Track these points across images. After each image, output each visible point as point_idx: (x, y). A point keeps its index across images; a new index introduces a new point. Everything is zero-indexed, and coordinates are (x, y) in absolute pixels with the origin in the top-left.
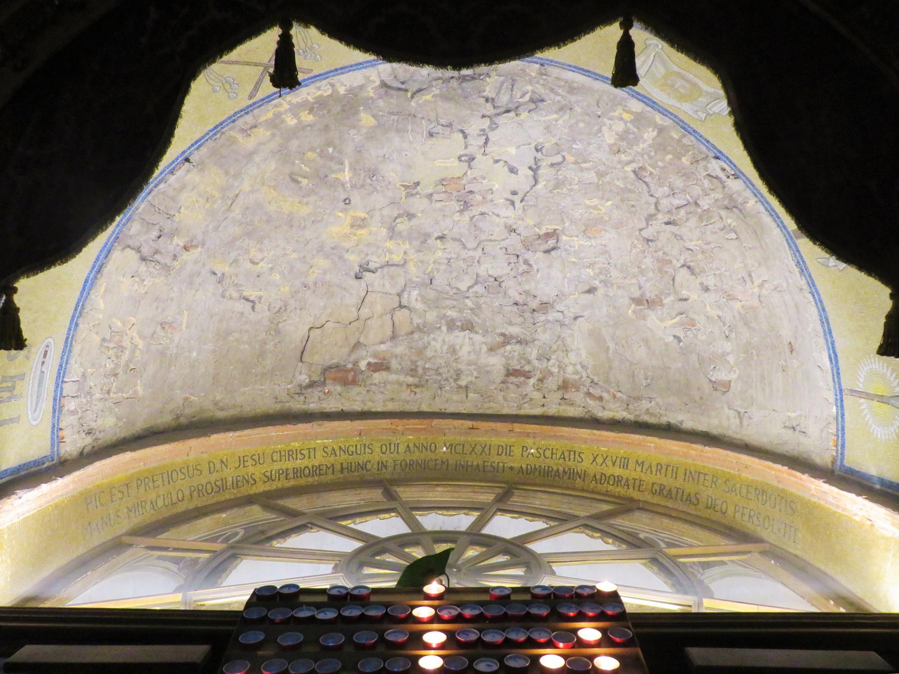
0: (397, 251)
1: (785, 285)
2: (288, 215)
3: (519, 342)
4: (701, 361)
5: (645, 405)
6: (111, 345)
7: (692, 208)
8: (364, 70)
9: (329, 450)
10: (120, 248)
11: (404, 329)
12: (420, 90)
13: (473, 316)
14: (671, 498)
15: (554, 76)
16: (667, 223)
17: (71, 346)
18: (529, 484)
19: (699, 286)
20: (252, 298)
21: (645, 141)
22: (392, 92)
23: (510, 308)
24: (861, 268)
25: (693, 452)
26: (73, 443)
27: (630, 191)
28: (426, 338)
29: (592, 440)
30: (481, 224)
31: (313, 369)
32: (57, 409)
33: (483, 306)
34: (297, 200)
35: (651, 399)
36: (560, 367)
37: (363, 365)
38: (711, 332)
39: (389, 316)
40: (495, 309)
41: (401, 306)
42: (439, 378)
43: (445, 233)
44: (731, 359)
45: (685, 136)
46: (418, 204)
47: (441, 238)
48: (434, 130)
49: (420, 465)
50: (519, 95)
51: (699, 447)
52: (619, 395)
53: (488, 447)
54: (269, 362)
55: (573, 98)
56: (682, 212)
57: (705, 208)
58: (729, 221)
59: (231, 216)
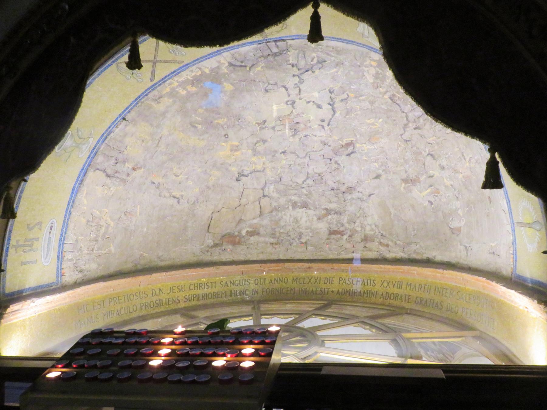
0: (259, 162)
1: (480, 158)
2: (193, 147)
4: (444, 215)
5: (414, 247)
6: (93, 224)
9: (224, 283)
10: (93, 170)
12: (253, 65)
16: (415, 129)
17: (68, 224)
24: (466, 134)
25: (439, 275)
26: (69, 277)
27: (391, 111)
29: (381, 272)
30: (306, 142)
32: (60, 257)
33: (313, 192)
36: (362, 227)
37: (244, 233)
38: (449, 196)
39: (258, 202)
41: (264, 196)
42: (289, 238)
44: (460, 212)
46: (268, 134)
47: (284, 152)
48: (267, 88)
50: (310, 60)
51: (441, 271)
52: (398, 242)
53: (319, 279)
55: (342, 57)
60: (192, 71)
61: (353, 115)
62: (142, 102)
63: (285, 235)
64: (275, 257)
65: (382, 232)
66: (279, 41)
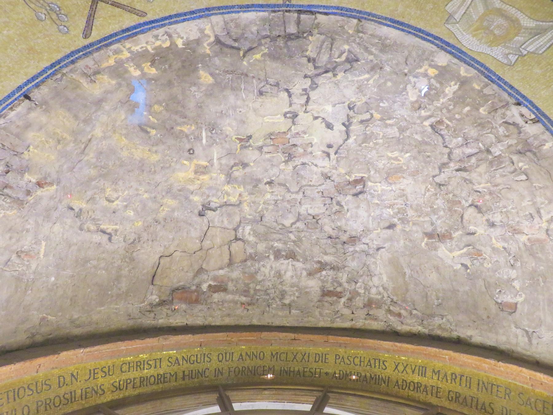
2: (140, 162)
3: (333, 268)
4: (488, 286)
5: (437, 321)
7: (484, 155)
8: (198, 21)
11: (238, 258)
12: (250, 49)
13: (295, 247)
14: (467, 405)
15: (370, 33)
16: (457, 170)
18: (342, 388)
19: (485, 223)
20: (109, 231)
21: (446, 95)
22: (226, 50)
23: (325, 241)
27: (426, 143)
28: (257, 265)
29: (394, 351)
30: (302, 173)
31: (163, 290)
33: (304, 239)
34: (147, 148)
35: (442, 317)
36: (365, 289)
37: (204, 287)
38: (497, 261)
39: (227, 247)
40: (313, 242)
41: (237, 239)
42: (268, 297)
43: (273, 179)
45: (486, 85)
46: (251, 155)
47: (270, 183)
48: (264, 89)
49: (251, 372)
51: (492, 362)
52: (414, 312)
53: (307, 354)
54: (124, 285)
55: (384, 57)
56: (473, 160)
57: (497, 154)
58: (521, 164)
59: (86, 158)
60: (156, 37)
61: (371, 143)
62: (64, 74)
63: (262, 293)
64: (246, 322)
65: (392, 297)
66: (305, 12)
